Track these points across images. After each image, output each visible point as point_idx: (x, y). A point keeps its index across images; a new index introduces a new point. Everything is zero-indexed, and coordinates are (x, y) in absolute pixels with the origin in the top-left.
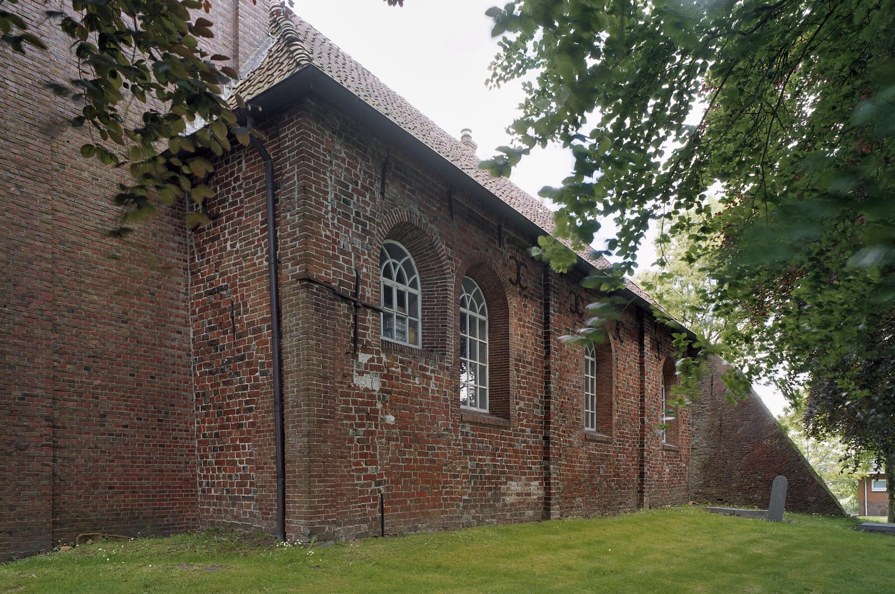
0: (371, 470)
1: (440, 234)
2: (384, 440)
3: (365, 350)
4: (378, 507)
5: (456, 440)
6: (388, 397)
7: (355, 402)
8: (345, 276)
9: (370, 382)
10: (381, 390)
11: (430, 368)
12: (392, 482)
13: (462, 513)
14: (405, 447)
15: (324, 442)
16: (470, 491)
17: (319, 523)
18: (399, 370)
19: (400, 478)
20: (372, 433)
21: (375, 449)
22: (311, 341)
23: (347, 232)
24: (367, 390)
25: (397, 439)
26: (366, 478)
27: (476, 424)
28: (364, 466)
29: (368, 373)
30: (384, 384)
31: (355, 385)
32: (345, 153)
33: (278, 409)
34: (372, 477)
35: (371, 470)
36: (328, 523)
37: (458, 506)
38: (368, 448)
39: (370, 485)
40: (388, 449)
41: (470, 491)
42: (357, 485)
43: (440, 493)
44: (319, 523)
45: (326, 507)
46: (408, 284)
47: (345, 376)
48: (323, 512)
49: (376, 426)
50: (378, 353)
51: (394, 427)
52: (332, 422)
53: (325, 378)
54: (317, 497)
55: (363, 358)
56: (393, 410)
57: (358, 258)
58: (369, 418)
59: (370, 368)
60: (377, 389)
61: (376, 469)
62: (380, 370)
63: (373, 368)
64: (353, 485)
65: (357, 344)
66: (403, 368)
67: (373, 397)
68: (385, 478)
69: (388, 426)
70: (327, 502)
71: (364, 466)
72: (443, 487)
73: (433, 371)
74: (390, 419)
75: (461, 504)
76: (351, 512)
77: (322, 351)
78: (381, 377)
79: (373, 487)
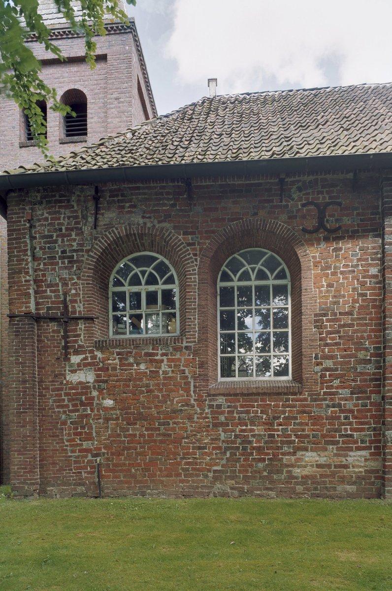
0: (86, 445)
1: (175, 228)
2: (101, 421)
3: (77, 353)
4: (96, 474)
5: (201, 414)
6: (103, 385)
7: (67, 394)
8: (53, 303)
9: (87, 377)
10: (95, 381)
11: (160, 352)
12: (112, 454)
13: (213, 483)
14: (128, 424)
15: (23, 426)
16: (224, 462)
17: (18, 483)
18: (117, 361)
19: (123, 450)
20: (87, 416)
21: (91, 428)
22: (11, 358)
23: (54, 269)
24: (80, 383)
25: (117, 419)
26: (80, 451)
27: (229, 395)
28: (78, 442)
29: (80, 370)
30: (98, 376)
31: (67, 382)
32: (47, 213)
33: (261, 391)
34: (87, 451)
35: (86, 445)
36: (27, 484)
37: (206, 476)
38: (83, 428)
39: (86, 457)
40: (107, 427)
41: (224, 462)
42: (71, 456)
43: (179, 464)
44: (18, 483)
45: (24, 472)
46: (143, 282)
47: (56, 376)
48: (21, 476)
49: (92, 410)
50: (91, 352)
51: (113, 409)
52: (30, 412)
53: (24, 382)
54: (17, 465)
55: (75, 359)
56: (111, 395)
57: (65, 285)
58: (82, 404)
59: (80, 366)
60: (92, 381)
61: (93, 444)
62: (94, 365)
63: (86, 365)
64: (66, 457)
65: (66, 351)
66: (120, 360)
67: (89, 387)
68: (103, 450)
69: (106, 409)
70: (26, 469)
71: (78, 442)
72: (182, 459)
73: (163, 355)
74: (109, 403)
75: (211, 475)
76: (65, 476)
77: (21, 363)
78: (95, 371)
79: (90, 458)
